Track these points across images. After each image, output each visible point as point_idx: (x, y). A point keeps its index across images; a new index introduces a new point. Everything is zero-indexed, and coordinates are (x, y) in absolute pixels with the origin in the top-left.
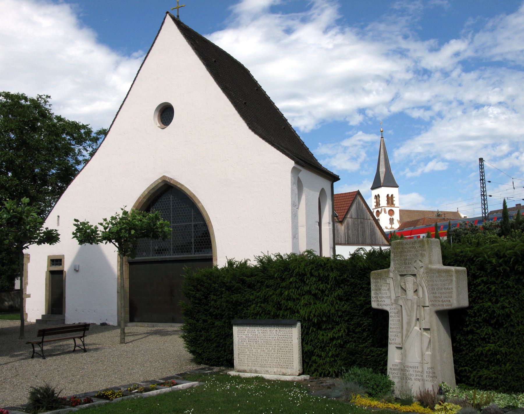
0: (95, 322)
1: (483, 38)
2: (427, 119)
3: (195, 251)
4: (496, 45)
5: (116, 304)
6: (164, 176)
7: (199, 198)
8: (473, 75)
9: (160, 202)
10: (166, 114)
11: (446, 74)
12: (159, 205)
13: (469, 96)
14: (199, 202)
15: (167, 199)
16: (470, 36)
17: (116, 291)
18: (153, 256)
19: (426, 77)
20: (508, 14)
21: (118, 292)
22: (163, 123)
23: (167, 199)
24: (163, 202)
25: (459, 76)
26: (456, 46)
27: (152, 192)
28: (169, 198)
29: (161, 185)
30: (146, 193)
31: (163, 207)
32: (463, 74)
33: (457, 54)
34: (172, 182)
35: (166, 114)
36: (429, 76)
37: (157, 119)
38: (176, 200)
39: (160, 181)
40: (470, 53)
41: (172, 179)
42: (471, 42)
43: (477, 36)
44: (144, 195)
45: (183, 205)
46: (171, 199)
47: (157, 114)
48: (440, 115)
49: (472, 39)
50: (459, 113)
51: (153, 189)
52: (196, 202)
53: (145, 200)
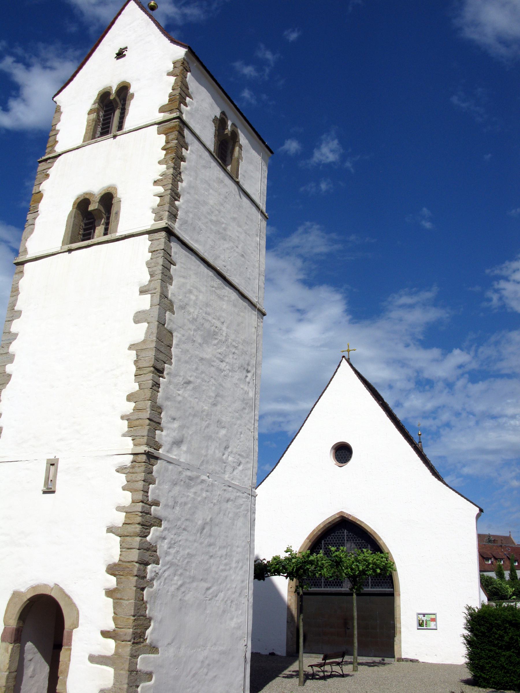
0: (259, 651)
1: (486, 351)
2: (434, 429)
3: (372, 585)
4: (502, 360)
5: (286, 634)
6: (341, 512)
7: (380, 535)
8: (480, 386)
9: (333, 536)
10: (343, 452)
11: (449, 385)
12: (332, 538)
13: (479, 407)
14: (381, 539)
15: (340, 533)
16: (473, 348)
17: (286, 620)
18: (324, 587)
19: (427, 387)
20: (510, 330)
21: (287, 622)
22: (338, 461)
23: (340, 533)
24: (336, 536)
25: (465, 387)
26: (458, 357)
27: (327, 526)
28: (343, 533)
29: (338, 520)
30: (322, 526)
31: (336, 541)
32: (470, 385)
33: (460, 367)
34: (350, 518)
35: (343, 452)
36: (432, 387)
37: (332, 456)
38: (350, 535)
39: (337, 516)
40: (474, 365)
41: (350, 515)
42: (476, 356)
43: (481, 349)
44: (319, 529)
45: (359, 540)
46: (345, 534)
47: (333, 451)
48: (448, 425)
49: (476, 351)
50: (472, 423)
51: (330, 523)
52: (377, 539)
53: (320, 533)
